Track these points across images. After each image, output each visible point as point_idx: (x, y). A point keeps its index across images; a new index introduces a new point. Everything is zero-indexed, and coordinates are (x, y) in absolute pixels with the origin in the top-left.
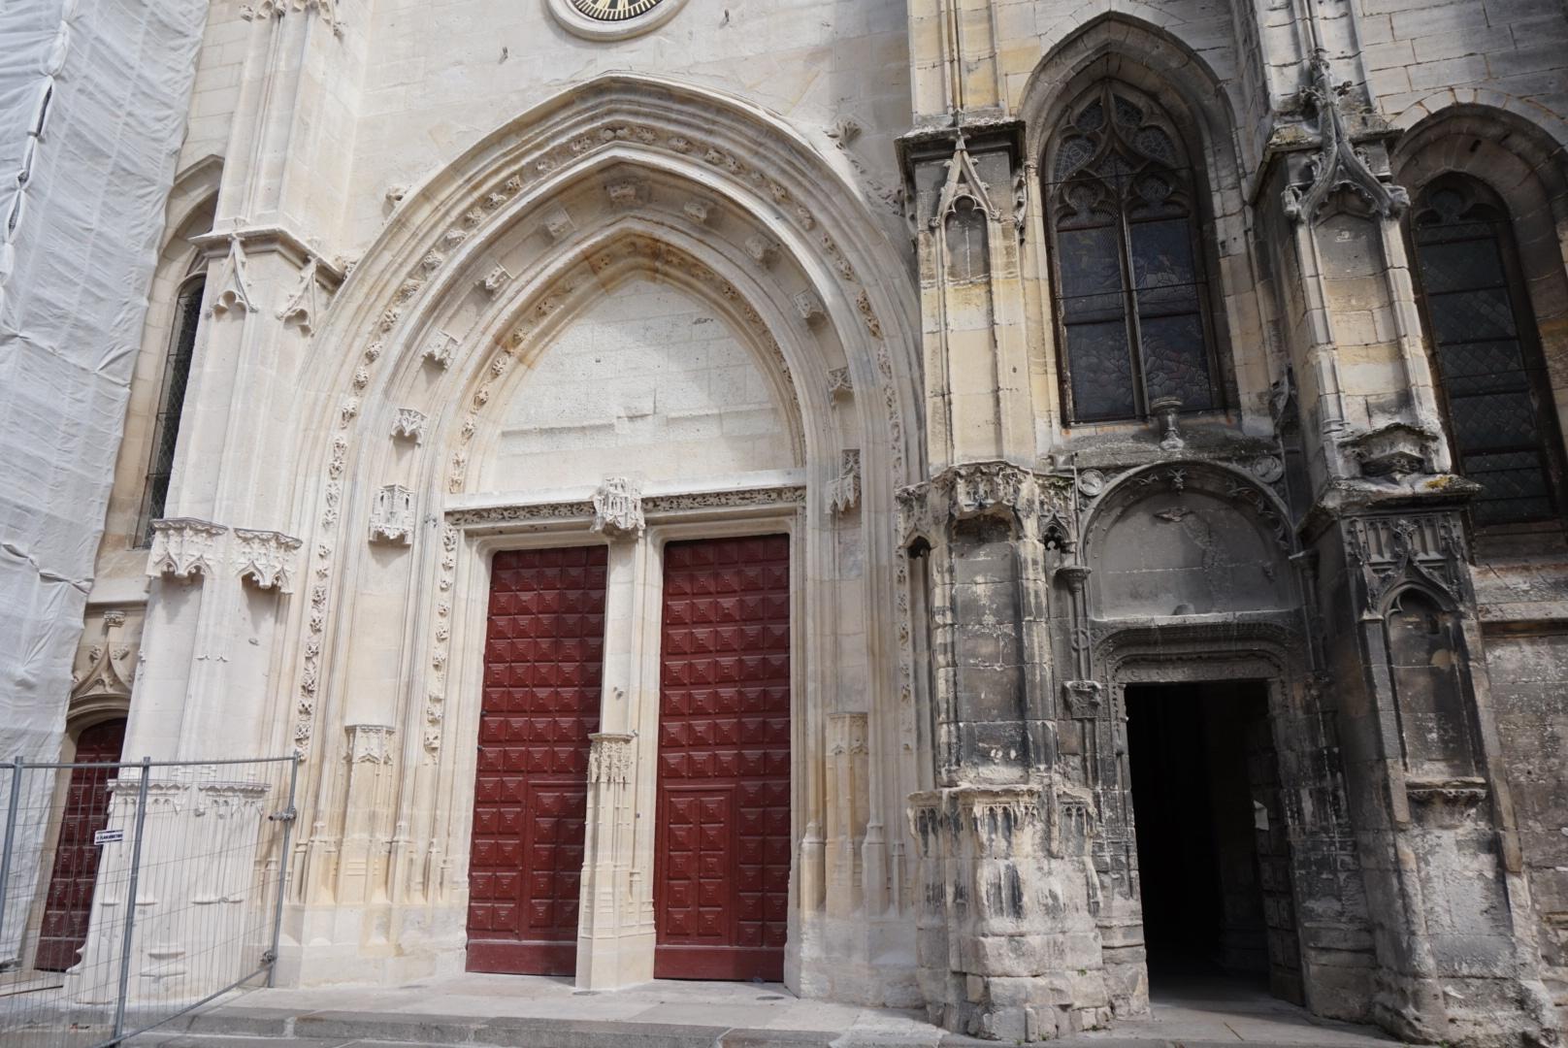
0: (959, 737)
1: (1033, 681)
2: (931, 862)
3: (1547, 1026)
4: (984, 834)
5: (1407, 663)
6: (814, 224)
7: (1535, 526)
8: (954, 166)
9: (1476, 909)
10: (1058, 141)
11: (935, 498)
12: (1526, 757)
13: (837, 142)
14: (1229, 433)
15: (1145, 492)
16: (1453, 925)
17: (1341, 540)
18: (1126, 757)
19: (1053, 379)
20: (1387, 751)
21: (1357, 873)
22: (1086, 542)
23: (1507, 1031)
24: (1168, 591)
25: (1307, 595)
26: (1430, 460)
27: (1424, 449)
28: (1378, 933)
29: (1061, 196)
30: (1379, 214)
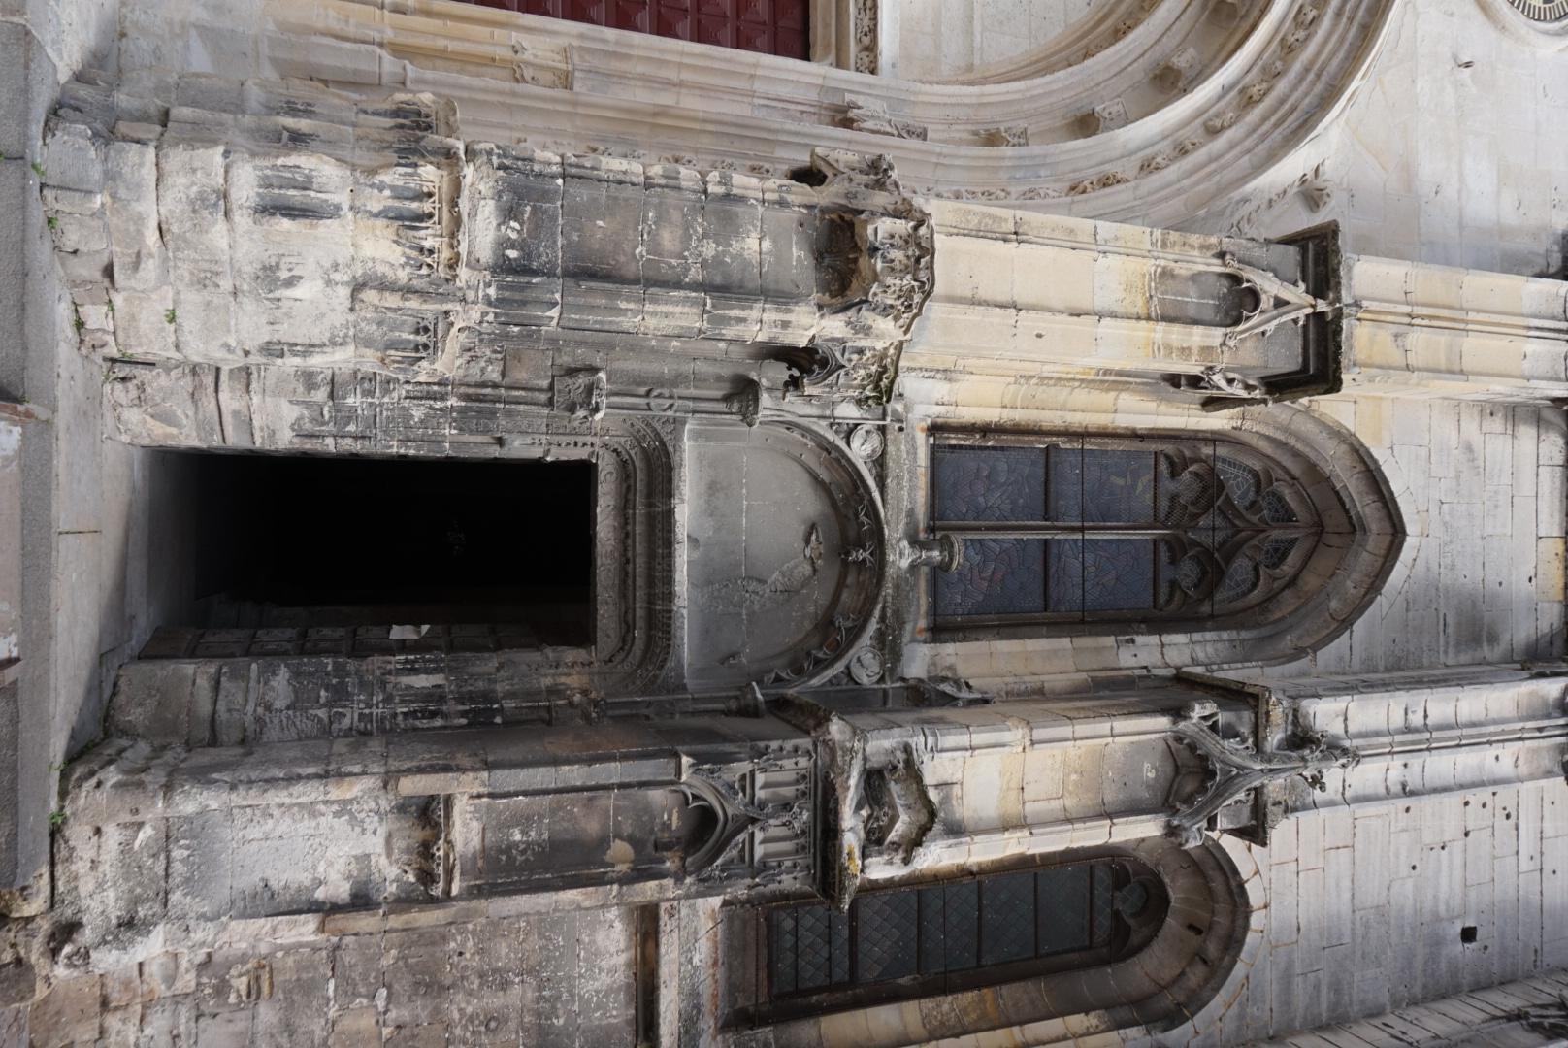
0: (540, 174)
1: (618, 295)
2: (352, 116)
3: (94, 955)
4: (393, 177)
5: (617, 809)
6: (1213, 132)
7: (763, 975)
8: (1297, 294)
9: (268, 873)
10: (1257, 466)
11: (881, 199)
12: (481, 952)
13: (1310, 176)
14: (909, 627)
15: (848, 509)
16: (245, 841)
17: (785, 739)
18: (495, 452)
19: (992, 415)
20: (500, 775)
21: (326, 732)
22: (790, 426)
23: (85, 903)
24: (717, 530)
25: (704, 700)
26: (880, 853)
27: (895, 847)
28: (239, 751)
29: (1197, 460)
30: (1175, 812)
